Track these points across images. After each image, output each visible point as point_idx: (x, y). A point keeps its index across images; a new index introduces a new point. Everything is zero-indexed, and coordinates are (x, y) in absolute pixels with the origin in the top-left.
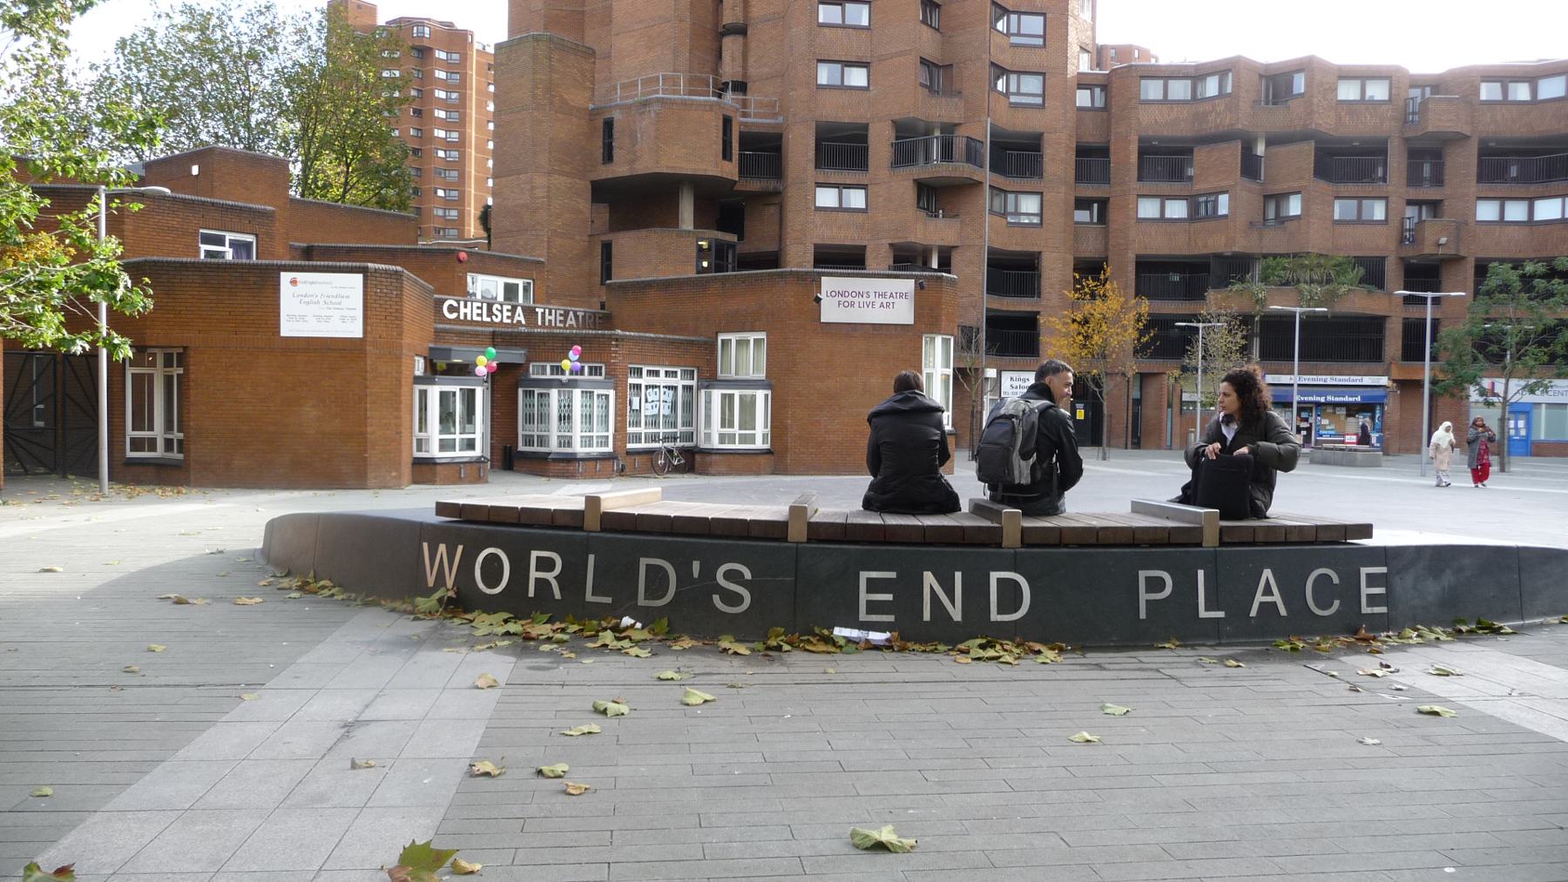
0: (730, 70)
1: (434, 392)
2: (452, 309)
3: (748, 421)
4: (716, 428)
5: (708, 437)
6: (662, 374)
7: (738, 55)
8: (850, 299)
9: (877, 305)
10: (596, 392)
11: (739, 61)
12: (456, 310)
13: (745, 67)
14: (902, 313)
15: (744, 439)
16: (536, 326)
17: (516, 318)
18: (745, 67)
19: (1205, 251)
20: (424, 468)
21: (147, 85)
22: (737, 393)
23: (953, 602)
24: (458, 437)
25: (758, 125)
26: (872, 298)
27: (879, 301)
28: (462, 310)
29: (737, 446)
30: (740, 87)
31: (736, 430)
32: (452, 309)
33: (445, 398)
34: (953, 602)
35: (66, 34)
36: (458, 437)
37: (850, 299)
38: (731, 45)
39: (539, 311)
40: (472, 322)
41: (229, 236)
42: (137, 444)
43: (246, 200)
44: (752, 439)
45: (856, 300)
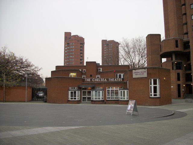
0: (185, 31)
1: (120, 91)
2: (94, 80)
3: (124, 96)
4: (70, 97)
5: (93, 98)
6: (118, 88)
7: (186, 28)
11: (186, 29)
13: (187, 30)
14: (145, 75)
15: (74, 99)
18: (187, 30)
22: (122, 91)
24: (73, 97)
28: (95, 80)
29: (111, 99)
30: (187, 33)
31: (122, 97)
32: (94, 80)
33: (121, 92)
38: (185, 27)
39: (109, 79)
42: (108, 98)
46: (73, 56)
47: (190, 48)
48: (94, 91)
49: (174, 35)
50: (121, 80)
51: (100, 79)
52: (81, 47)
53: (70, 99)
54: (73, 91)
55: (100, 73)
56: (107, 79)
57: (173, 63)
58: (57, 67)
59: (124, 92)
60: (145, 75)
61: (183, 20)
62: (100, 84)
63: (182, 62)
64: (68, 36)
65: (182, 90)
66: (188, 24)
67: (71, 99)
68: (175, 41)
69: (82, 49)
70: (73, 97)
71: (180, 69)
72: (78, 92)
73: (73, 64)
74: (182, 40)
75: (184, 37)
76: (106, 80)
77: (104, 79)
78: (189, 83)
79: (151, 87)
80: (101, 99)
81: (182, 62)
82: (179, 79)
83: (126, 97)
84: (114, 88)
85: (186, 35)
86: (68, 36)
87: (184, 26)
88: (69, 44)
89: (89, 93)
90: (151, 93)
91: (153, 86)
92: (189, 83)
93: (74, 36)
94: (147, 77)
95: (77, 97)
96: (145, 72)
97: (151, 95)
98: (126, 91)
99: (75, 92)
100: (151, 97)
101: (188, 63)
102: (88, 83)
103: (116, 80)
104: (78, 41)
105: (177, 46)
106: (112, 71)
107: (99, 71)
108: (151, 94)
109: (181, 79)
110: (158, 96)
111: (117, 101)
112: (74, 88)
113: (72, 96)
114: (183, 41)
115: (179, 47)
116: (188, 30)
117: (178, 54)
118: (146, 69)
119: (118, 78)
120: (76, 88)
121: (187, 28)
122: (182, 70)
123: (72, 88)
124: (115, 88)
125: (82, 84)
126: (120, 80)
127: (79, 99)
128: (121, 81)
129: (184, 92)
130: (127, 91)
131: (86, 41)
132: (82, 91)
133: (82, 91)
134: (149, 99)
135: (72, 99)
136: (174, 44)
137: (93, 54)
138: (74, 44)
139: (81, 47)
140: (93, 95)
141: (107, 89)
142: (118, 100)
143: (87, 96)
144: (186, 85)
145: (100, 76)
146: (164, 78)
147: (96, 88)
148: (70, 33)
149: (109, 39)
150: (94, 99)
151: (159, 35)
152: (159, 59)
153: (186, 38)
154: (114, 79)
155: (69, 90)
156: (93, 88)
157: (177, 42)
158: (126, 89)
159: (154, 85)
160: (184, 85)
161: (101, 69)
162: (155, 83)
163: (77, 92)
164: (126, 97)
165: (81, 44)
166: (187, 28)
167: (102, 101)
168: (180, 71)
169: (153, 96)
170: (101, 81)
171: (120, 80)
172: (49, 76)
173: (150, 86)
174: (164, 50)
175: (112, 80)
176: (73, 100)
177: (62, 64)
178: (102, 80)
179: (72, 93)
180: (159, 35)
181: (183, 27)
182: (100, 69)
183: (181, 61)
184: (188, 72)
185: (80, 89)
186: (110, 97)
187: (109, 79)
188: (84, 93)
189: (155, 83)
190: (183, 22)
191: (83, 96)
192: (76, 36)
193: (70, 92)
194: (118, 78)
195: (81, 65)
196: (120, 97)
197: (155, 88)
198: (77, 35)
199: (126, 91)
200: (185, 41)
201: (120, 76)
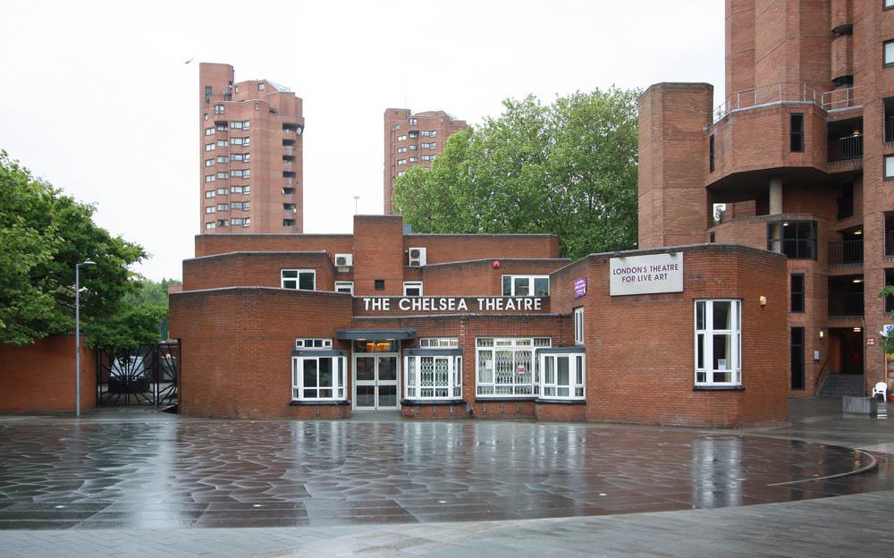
0: (838, 69)
1: (543, 356)
2: (405, 304)
4: (301, 386)
8: (631, 275)
9: (653, 277)
10: (435, 358)
11: (843, 59)
12: (410, 304)
13: (849, 62)
14: (674, 282)
16: (479, 311)
17: (460, 307)
18: (849, 62)
19: (865, 212)
20: (294, 407)
21: (76, 228)
23: (208, 481)
25: (838, 114)
26: (649, 272)
27: (654, 274)
28: (414, 304)
30: (847, 80)
31: (555, 385)
32: (405, 304)
34: (208, 481)
35: (552, 105)
36: (318, 388)
37: (631, 275)
38: (838, 47)
39: (481, 300)
40: (422, 312)
41: (299, 271)
43: (317, 249)
44: (567, 392)
45: (636, 275)
46: (248, 189)
47: (861, 153)
48: (418, 358)
49: (776, 87)
50: (536, 304)
51: (437, 301)
52: (286, 143)
53: (301, 398)
54: (317, 358)
55: (419, 273)
56: (472, 302)
57: (771, 228)
58: (359, 220)
59: (563, 364)
60: (674, 282)
61: (834, 12)
62: (442, 324)
63: (815, 224)
64: (217, 87)
65: (813, 354)
66: (856, 39)
67: (307, 394)
68: (789, 116)
69: (290, 153)
70: (318, 388)
71: (805, 254)
72: (340, 361)
73: (251, 226)
74: (820, 113)
75: (828, 98)
76: (463, 305)
77: (457, 301)
78: (843, 323)
79: (701, 337)
80: (451, 396)
81: (815, 224)
82: (798, 306)
83: (573, 384)
84: (514, 341)
85: (845, 89)
86: (217, 87)
87: (834, 44)
88: (225, 124)
89: (389, 370)
90: (701, 365)
91: (709, 333)
92: (843, 323)
93: (254, 86)
94: (682, 290)
95: (335, 387)
96: (673, 267)
97: (701, 377)
98: (572, 357)
99: (326, 364)
100: (697, 384)
101: (847, 224)
102: (380, 321)
103: (510, 305)
104: (272, 111)
105: (796, 144)
106: (487, 262)
107: (413, 263)
108: (701, 370)
109: (809, 302)
110: (734, 381)
111: (524, 406)
112: (318, 344)
113: (309, 381)
114: (828, 120)
115: (806, 149)
116: (856, 64)
117: (795, 183)
118: (680, 255)
119: (513, 294)
120: (327, 344)
121: (849, 53)
122: (816, 259)
123: (309, 344)
124: (518, 343)
125: (356, 324)
126: (533, 306)
127: (344, 398)
128: (533, 311)
129: (819, 366)
130: (579, 359)
131: (311, 116)
132: (355, 356)
133: (355, 356)
134: (691, 395)
135: (313, 394)
136: (779, 130)
137: (342, 188)
138: (251, 128)
139: (286, 143)
140: (411, 376)
141: (478, 349)
142: (532, 401)
143: (377, 383)
144: (833, 333)
145: (420, 288)
146: (763, 299)
147: (425, 343)
148: (230, 70)
149: (419, 105)
150: (418, 397)
151: (708, 89)
152: (700, 207)
153: (839, 106)
154: (505, 302)
155: (298, 353)
156: (408, 345)
157: (796, 121)
158: (570, 345)
159: (715, 328)
160: (822, 334)
161: (423, 251)
162: (721, 320)
163: (335, 360)
164: (573, 384)
165: (286, 126)
166: (849, 53)
167: (454, 403)
168: (803, 266)
169: (710, 382)
170: (439, 311)
171: (533, 306)
172: (177, 275)
173: (697, 332)
174: (729, 164)
175: (495, 305)
176: (318, 399)
177: (377, 208)
178: (447, 305)
179: (309, 365)
180: (708, 89)
181: (829, 46)
182: (416, 254)
183: (811, 218)
184: (847, 270)
185: (344, 345)
186: (489, 384)
187: (481, 300)
188: (365, 370)
189: (721, 320)
190: (834, 19)
191: (356, 383)
192: (259, 83)
193: (300, 360)
194: (513, 294)
195: (288, 231)
196: (543, 384)
197: (721, 346)
198: (264, 82)
199: (572, 357)
200: (836, 119)
201: (522, 287)
